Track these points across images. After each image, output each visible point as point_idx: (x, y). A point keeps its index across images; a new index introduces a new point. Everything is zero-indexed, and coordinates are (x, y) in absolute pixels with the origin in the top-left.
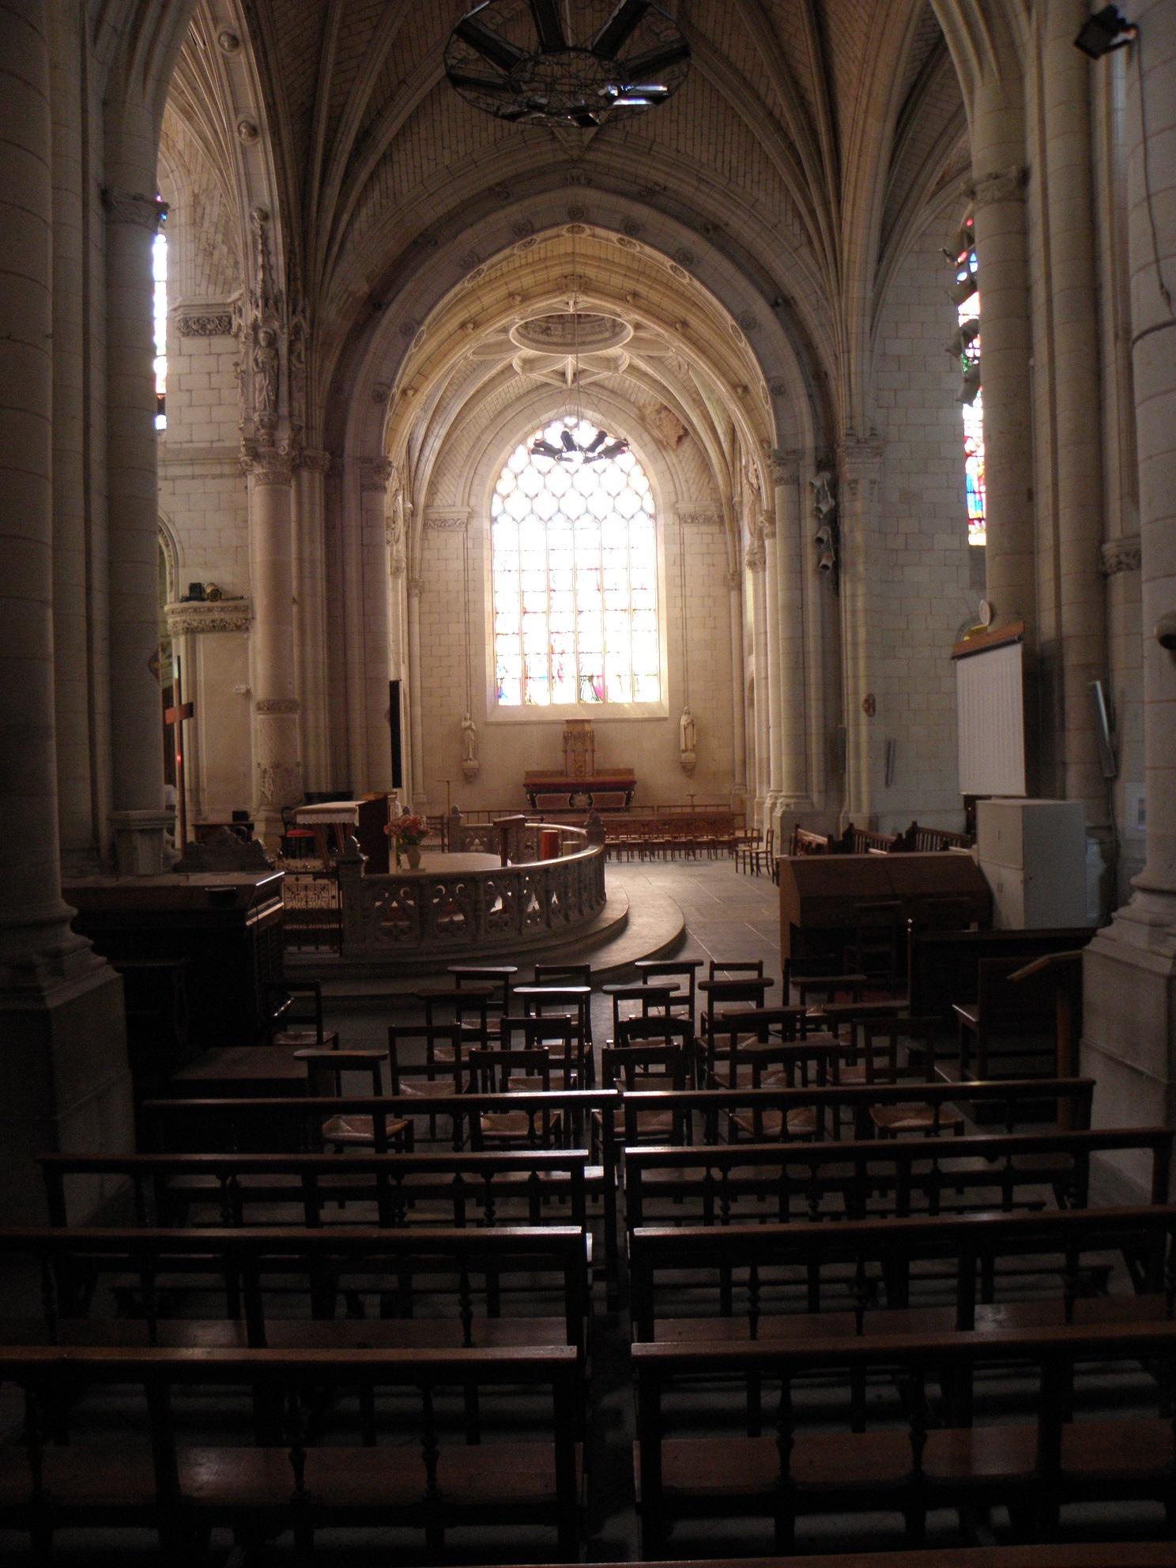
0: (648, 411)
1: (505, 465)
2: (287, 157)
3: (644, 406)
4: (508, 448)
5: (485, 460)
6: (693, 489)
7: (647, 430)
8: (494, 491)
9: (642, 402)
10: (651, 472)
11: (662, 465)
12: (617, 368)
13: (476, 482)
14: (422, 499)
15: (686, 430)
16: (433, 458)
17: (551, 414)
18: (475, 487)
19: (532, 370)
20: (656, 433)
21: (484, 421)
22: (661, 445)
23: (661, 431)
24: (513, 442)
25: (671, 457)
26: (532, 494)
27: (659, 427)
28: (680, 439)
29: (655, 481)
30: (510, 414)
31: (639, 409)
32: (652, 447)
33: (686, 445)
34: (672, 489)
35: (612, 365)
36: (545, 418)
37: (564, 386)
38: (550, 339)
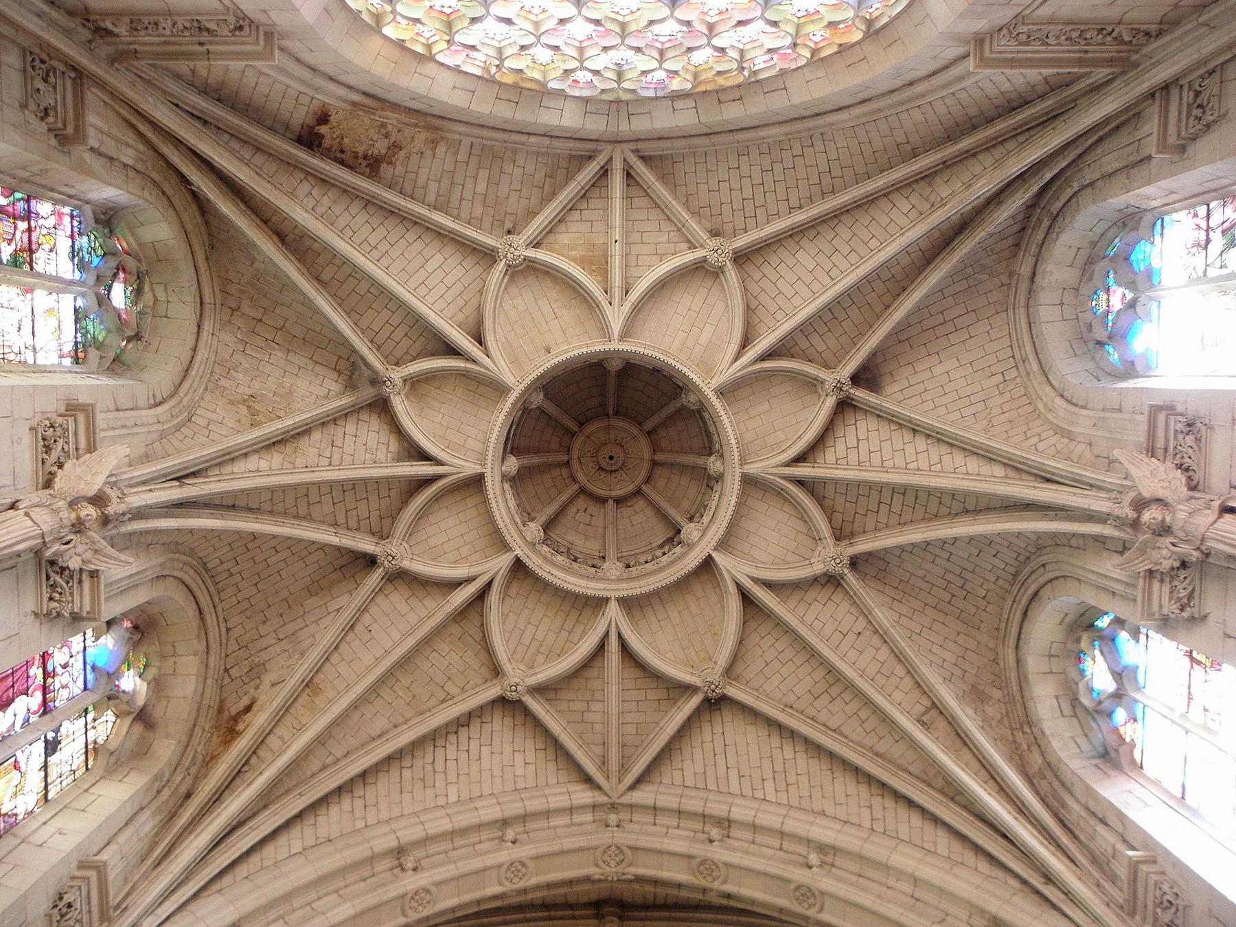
3: (434, 143)
9: (441, 150)
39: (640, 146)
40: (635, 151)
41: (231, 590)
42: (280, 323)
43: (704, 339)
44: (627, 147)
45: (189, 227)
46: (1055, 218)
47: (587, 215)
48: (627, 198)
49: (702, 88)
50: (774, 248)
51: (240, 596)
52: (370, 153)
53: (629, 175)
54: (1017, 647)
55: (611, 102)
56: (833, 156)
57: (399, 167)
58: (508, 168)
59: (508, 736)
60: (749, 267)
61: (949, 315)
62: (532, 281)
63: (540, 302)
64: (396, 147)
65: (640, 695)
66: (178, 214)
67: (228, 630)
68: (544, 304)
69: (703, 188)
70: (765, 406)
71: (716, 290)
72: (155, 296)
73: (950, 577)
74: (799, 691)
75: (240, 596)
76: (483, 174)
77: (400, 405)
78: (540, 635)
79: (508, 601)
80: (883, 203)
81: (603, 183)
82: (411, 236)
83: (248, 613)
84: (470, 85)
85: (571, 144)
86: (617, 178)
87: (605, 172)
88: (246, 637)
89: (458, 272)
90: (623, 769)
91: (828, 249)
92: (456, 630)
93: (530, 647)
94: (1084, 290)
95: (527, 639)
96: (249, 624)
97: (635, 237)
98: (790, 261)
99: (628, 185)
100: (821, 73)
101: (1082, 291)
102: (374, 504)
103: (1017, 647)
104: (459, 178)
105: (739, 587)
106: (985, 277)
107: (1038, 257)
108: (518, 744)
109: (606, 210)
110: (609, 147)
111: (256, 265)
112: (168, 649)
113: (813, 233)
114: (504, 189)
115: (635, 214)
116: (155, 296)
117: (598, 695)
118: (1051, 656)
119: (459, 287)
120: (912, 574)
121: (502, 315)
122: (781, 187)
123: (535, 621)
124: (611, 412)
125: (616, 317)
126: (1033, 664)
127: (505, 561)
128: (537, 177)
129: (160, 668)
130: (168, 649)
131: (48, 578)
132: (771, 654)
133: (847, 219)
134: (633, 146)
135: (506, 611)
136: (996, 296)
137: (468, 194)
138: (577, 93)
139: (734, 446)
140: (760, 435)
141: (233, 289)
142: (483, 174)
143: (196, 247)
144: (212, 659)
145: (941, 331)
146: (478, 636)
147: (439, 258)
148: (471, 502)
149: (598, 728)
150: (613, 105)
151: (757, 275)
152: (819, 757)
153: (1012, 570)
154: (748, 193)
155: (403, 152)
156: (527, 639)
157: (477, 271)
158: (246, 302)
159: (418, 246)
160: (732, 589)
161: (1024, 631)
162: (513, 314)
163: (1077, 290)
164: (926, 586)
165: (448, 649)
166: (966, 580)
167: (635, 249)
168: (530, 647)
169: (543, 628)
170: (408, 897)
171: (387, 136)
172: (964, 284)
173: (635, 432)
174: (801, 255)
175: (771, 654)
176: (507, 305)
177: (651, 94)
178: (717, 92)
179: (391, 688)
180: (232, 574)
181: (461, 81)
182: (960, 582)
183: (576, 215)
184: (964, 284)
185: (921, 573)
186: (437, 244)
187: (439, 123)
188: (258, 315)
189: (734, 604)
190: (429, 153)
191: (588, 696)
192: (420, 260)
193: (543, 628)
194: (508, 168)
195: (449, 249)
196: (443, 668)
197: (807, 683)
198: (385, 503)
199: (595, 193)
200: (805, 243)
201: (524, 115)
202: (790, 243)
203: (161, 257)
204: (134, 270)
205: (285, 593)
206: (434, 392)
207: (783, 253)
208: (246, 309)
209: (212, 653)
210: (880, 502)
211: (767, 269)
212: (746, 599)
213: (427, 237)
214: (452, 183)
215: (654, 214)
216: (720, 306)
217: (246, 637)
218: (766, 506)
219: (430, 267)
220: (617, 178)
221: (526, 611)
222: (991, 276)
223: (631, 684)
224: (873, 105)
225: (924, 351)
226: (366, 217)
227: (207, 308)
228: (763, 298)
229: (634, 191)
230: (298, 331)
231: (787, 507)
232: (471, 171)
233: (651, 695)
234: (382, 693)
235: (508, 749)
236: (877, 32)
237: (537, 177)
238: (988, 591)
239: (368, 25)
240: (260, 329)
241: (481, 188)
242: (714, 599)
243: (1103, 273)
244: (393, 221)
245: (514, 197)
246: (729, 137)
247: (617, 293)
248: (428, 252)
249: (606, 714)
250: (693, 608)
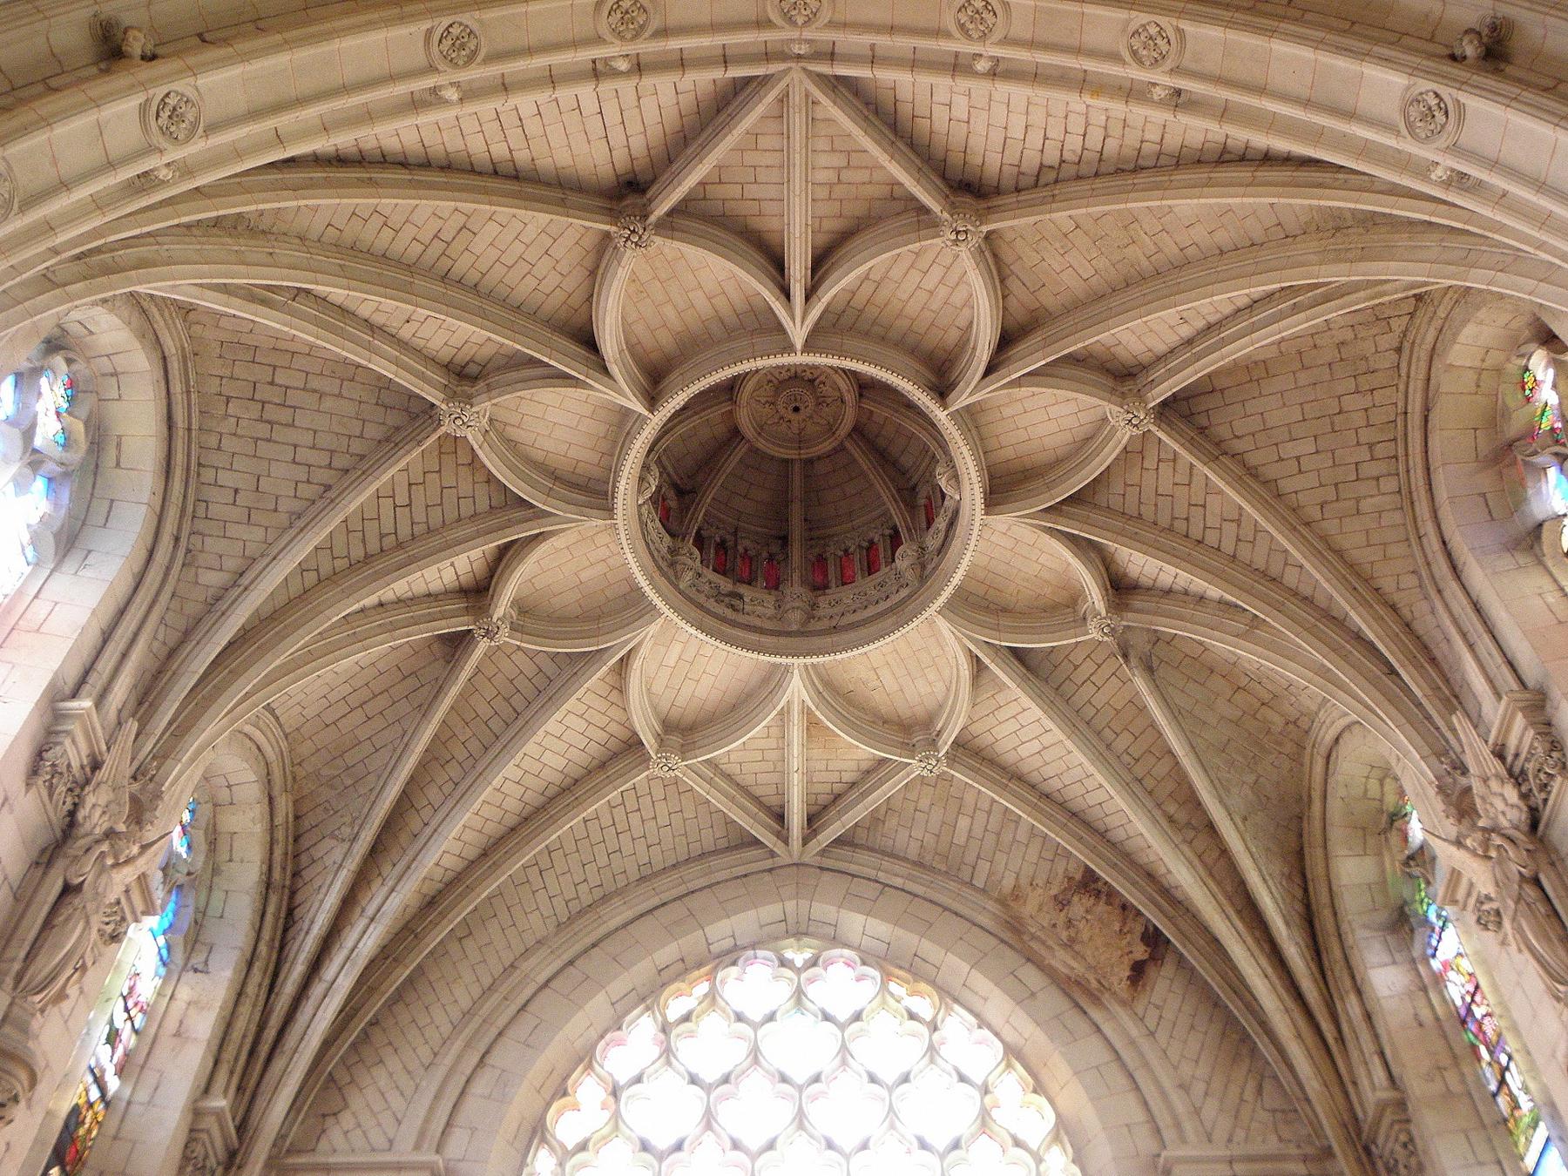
0: (1032, 907)
1: (585, 1058)
2: (269, 918)
3: (1016, 894)
4: (598, 1005)
5: (521, 1030)
6: (1210, 1109)
7: (1030, 959)
8: (537, 1132)
9: (1008, 883)
10: (1059, 1070)
11: (1094, 1049)
12: (933, 744)
13: (480, 1087)
14: (276, 1111)
15: (1153, 939)
16: (345, 983)
17: (744, 923)
18: (471, 1105)
19: (685, 751)
20: (1061, 960)
21: (536, 924)
22: (1079, 992)
23: (1078, 955)
24: (618, 986)
25: (1119, 1023)
26: (662, 1142)
27: (1070, 944)
28: (1138, 972)
29: (1075, 1098)
30: (616, 915)
31: (1002, 902)
32: (1052, 1000)
33: (1163, 982)
34: (1139, 1115)
35: (918, 738)
36: (720, 932)
37: (779, 848)
38: (741, 618)
39: (768, 864)
40: (772, 854)
41: (1378, 417)
42: (1238, 697)
43: (676, 649)
44: (784, 859)
45: (1319, 852)
46: (268, 885)
47: (835, 777)
48: (781, 793)
49: (704, 970)
50: (595, 762)
51: (1366, 401)
52: (1092, 900)
53: (780, 817)
54: (164, 358)
55: (806, 934)
56: (541, 895)
57: (1061, 871)
58: (929, 840)
59: (977, 143)
60: (623, 734)
61: (359, 716)
62: (905, 712)
63: (896, 687)
64: (1062, 903)
65: (753, 191)
66: (1328, 876)
67: (1399, 350)
68: (890, 684)
69: (689, 814)
70: (584, 576)
71: (664, 706)
72: (1382, 785)
73: (284, 415)
74: (493, 229)
75: (1366, 401)
76: (960, 839)
77: (1095, 595)
78: (915, 276)
79: (962, 322)
80: (472, 853)
81: (814, 809)
82: (1056, 784)
83: (1362, 366)
84: (966, 995)
85: (853, 868)
86: (796, 819)
87: (813, 820)
88: (1374, 331)
89: (1000, 732)
90: (783, 99)
91: (530, 781)
92: (1048, 300)
93: (938, 280)
94: (206, 810)
95: (937, 272)
96: (1367, 347)
97: (773, 755)
98: (574, 754)
99: (782, 807)
100: (579, 1044)
101: (210, 805)
102: (1149, 480)
103: (164, 358)
104: (990, 839)
105: (605, 370)
106: (326, 772)
107: (272, 828)
108: (959, 132)
109: (810, 782)
110: (806, 860)
111: (1251, 778)
112: (1488, 381)
113: (551, 791)
114: (936, 816)
115: (775, 778)
116: (1382, 785)
117: (822, 193)
118: (115, 374)
119: (1001, 715)
120: (340, 395)
121: (946, 673)
122: (596, 836)
123: (922, 296)
124: (797, 467)
125: (797, 690)
126: (140, 361)
127: (963, 398)
128: (894, 821)
129: (1508, 360)
130: (1488, 381)
131: (1545, 801)
132: (544, 266)
133: (511, 820)
134: (778, 861)
135: (966, 311)
136: (305, 749)
137: (981, 817)
138: (846, 952)
139: (623, 536)
140: (592, 551)
141: (1289, 748)
142: (960, 839)
143: (1317, 824)
144: (1430, 338)
145: (365, 694)
146: (1013, 284)
147: (1024, 751)
148: (1008, 453)
149: (822, 144)
150: (803, 928)
151: (614, 728)
152: (447, 154)
153: (208, 475)
154: (635, 819)
155: (1054, 891)
156: (937, 272)
157: (976, 729)
158: (1277, 729)
159: (1048, 771)
160: (614, 369)
161: (164, 402)
162: (932, 676)
163: (215, 805)
164: (315, 383)
165: (1064, 276)
166: (261, 420)
167: (773, 743)
168: (938, 280)
169: (908, 286)
170: (1169, 64)
171: (1069, 923)
172: (350, 758)
173: (761, 444)
174: (559, 763)
175: (544, 266)
176: (939, 688)
177: (760, 953)
178: (687, 970)
179: (1160, 250)
180: (1371, 446)
181: (978, 1005)
182: (271, 413)
183: (847, 777)
184: (350, 758)
185: (328, 403)
186: (1025, 768)
187: (1007, 936)
188: (1264, 710)
189: (610, 342)
190: (1024, 881)
191: (839, 191)
192: (1047, 756)
193: (908, 286)
194: (929, 840)
195: (1010, 758)
196: (1074, 252)
197: (479, 245)
198: (1133, 477)
199: (823, 800)
200: (556, 778)
201: (909, 940)
202: (576, 772)
203: (1360, 833)
204: (1394, 832)
205: (1304, 378)
206: (1048, 591)
207: (583, 759)
208: (1278, 721)
209: (1428, 346)
210: (410, 505)
211: (601, 736)
212: (588, 341)
213: (1035, 778)
214: (998, 834)
215: (748, 780)
216: (658, 687)
217: (1374, 331)
218: (571, 453)
219: (1035, 746)
220: (796, 819)
221: (934, 307)
222: (317, 773)
223: (769, 208)
224: (514, 1008)
225: (381, 666)
226: (1107, 820)
227: (1323, 751)
228: (601, 705)
229: (773, 801)
230: (1217, 683)
231: (539, 456)
232: (974, 844)
233: (735, 191)
234: (1177, 251)
235: (979, 125)
236: (534, 1132)
237: (894, 821)
238: (227, 415)
239: (1067, 1133)
240: (1267, 697)
241: (963, 823)
242: (639, 329)
243: (195, 845)
244: (1074, 806)
245: (924, 803)
246: (665, 897)
247: (796, 709)
248: (1037, 762)
249: (809, 167)
250: (669, 311)
